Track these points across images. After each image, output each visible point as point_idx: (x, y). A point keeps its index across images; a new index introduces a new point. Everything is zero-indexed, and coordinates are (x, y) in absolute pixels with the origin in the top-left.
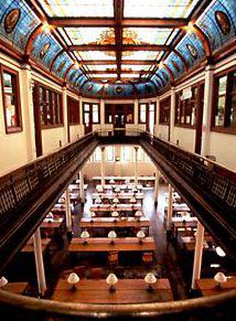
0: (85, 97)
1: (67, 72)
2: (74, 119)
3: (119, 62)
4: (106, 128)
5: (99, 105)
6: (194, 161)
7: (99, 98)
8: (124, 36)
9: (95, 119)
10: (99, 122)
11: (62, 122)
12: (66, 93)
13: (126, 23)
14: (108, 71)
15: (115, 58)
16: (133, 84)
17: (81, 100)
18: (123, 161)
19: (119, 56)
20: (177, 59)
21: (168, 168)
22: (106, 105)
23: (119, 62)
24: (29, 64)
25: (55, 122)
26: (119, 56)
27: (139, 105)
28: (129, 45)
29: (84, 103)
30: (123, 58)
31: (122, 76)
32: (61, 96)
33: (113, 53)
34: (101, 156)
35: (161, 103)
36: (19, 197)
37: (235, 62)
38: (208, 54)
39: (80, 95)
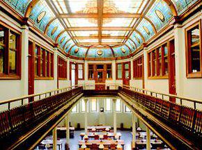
0: (72, 57)
1: (58, 36)
2: (62, 74)
3: (100, 28)
4: (90, 84)
5: (83, 64)
6: (171, 105)
7: (84, 59)
8: (105, 5)
9: (80, 76)
10: (83, 79)
11: (52, 76)
12: (56, 54)
13: (95, 29)
14: (91, 37)
15: (96, 25)
16: (111, 48)
17: (68, 60)
18: (155, 20)
19: (100, 23)
20: (138, 36)
21: (145, 113)
22: (65, 131)
23: (100, 28)
24: (28, 25)
25: (47, 74)
26: (100, 23)
27: (117, 64)
28: (108, 14)
29: (71, 63)
30: (103, 26)
31: (104, 41)
32: (52, 55)
33: (93, 20)
34: (84, 109)
35: (134, 62)
36: (10, 51)
37: (201, 17)
38: (175, 15)
39: (67, 56)
